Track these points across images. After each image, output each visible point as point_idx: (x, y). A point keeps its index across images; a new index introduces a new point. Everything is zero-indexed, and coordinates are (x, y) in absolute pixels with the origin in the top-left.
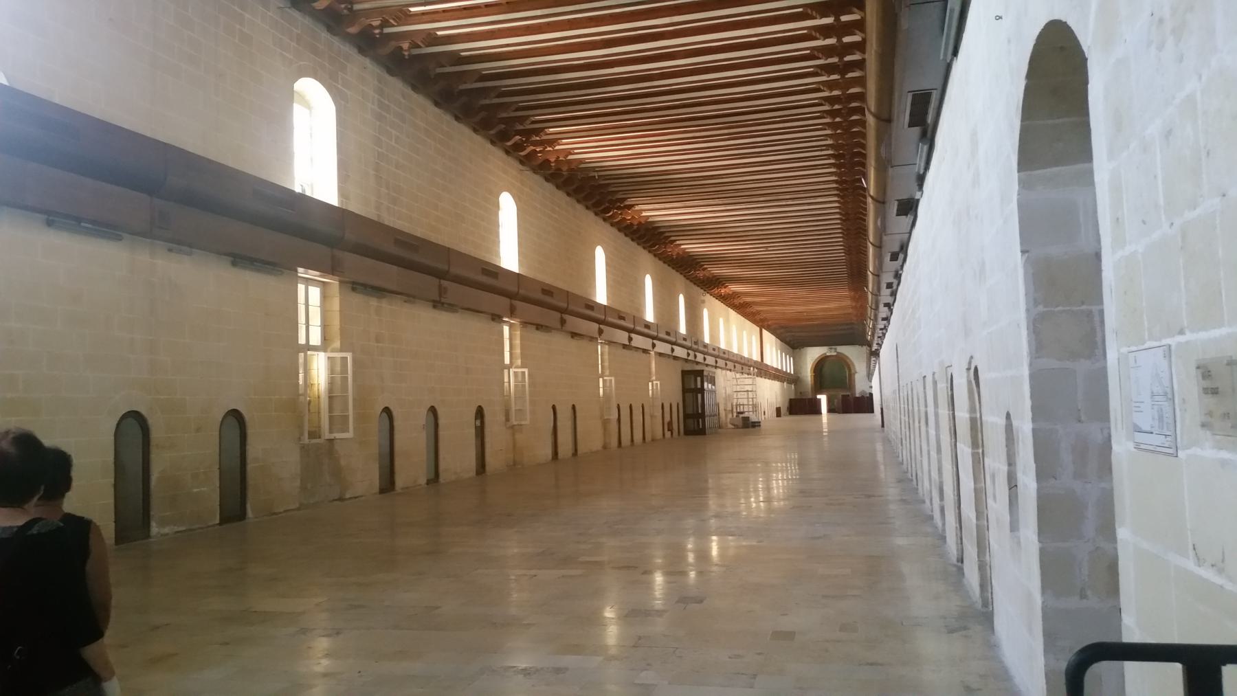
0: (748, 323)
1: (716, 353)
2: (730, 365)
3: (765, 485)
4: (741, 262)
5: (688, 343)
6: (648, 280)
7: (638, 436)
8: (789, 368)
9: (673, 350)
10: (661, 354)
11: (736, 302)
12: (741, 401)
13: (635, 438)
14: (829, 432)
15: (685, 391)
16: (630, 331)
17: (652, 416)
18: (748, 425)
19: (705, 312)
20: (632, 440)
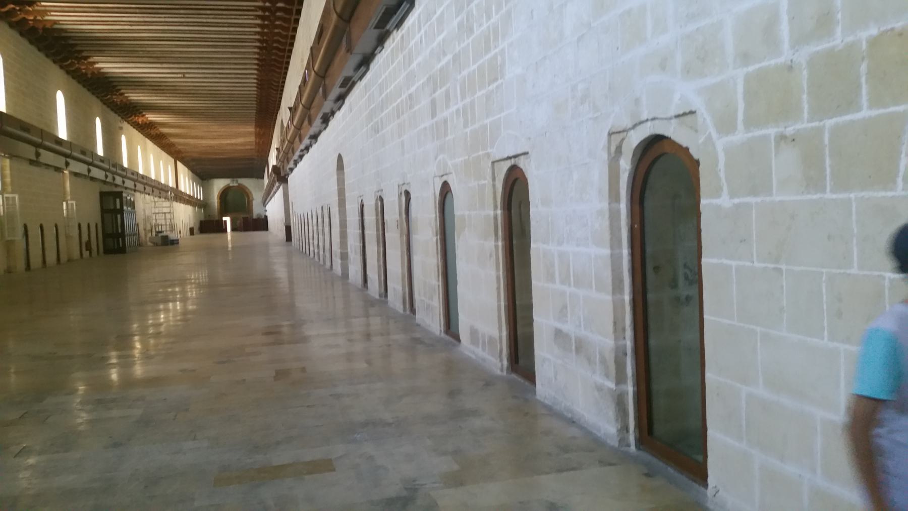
0: (164, 154)
1: (135, 177)
2: (149, 189)
3: (169, 305)
4: (156, 87)
5: (106, 166)
6: (60, 97)
7: (51, 257)
8: (199, 194)
9: (89, 171)
10: (76, 174)
11: (153, 132)
12: (159, 222)
13: (48, 259)
14: (232, 247)
15: (104, 211)
16: (37, 146)
17: (68, 237)
18: (167, 243)
19: (123, 139)
20: (44, 262)
